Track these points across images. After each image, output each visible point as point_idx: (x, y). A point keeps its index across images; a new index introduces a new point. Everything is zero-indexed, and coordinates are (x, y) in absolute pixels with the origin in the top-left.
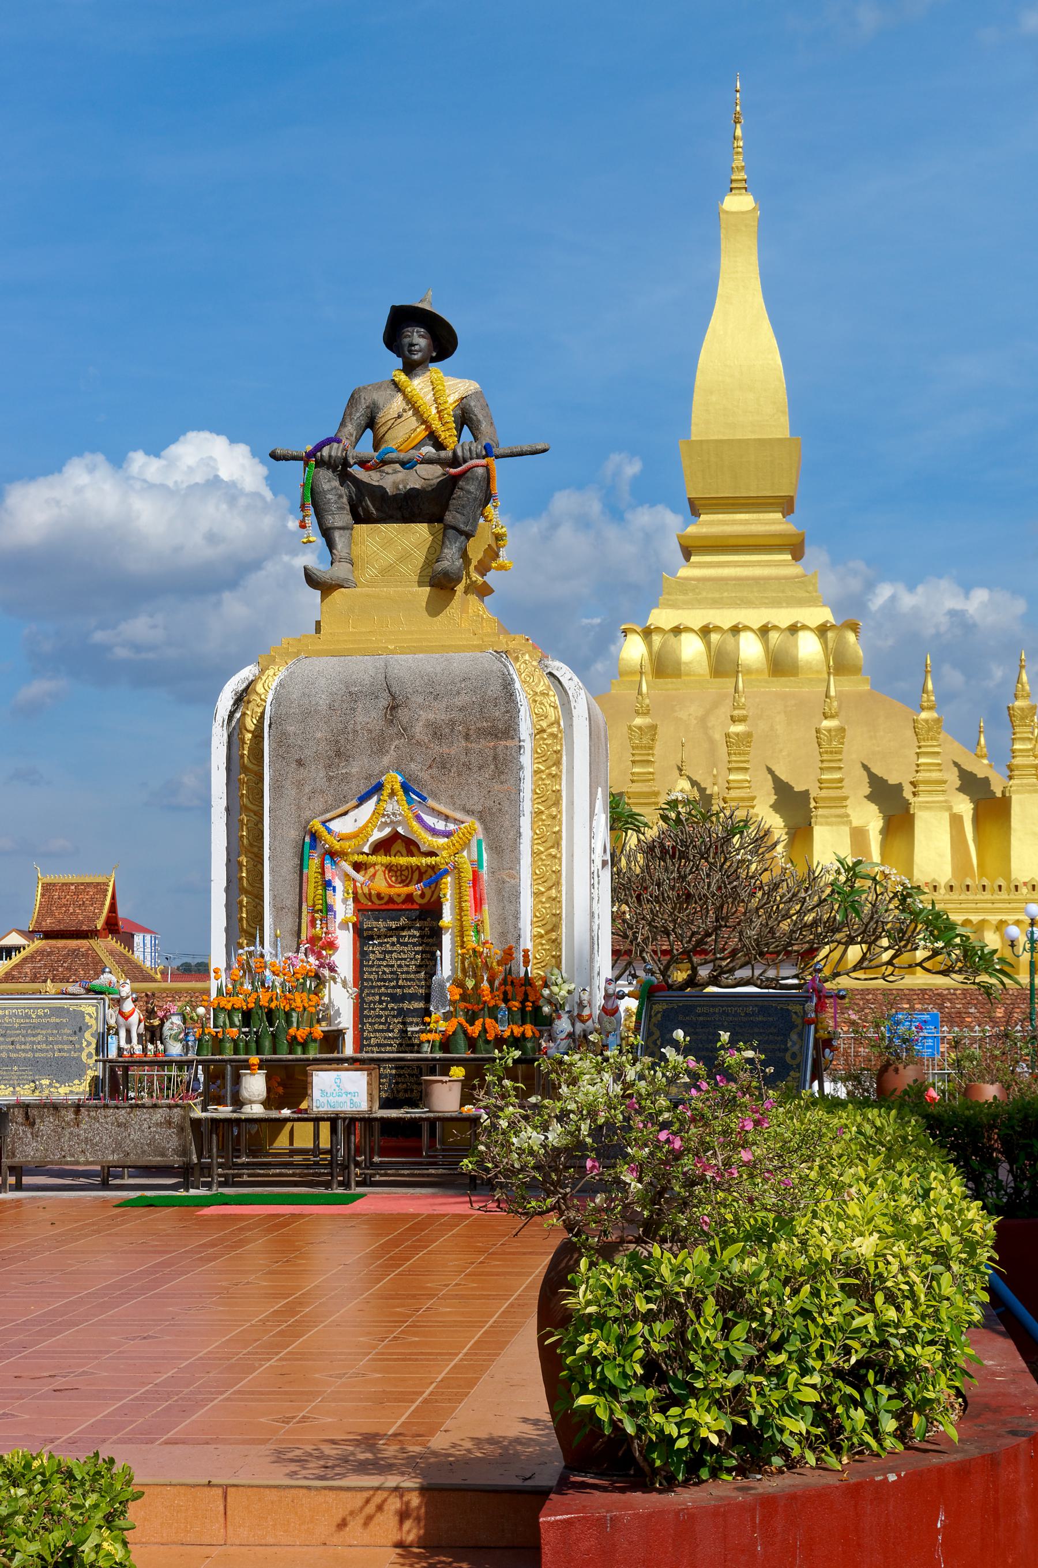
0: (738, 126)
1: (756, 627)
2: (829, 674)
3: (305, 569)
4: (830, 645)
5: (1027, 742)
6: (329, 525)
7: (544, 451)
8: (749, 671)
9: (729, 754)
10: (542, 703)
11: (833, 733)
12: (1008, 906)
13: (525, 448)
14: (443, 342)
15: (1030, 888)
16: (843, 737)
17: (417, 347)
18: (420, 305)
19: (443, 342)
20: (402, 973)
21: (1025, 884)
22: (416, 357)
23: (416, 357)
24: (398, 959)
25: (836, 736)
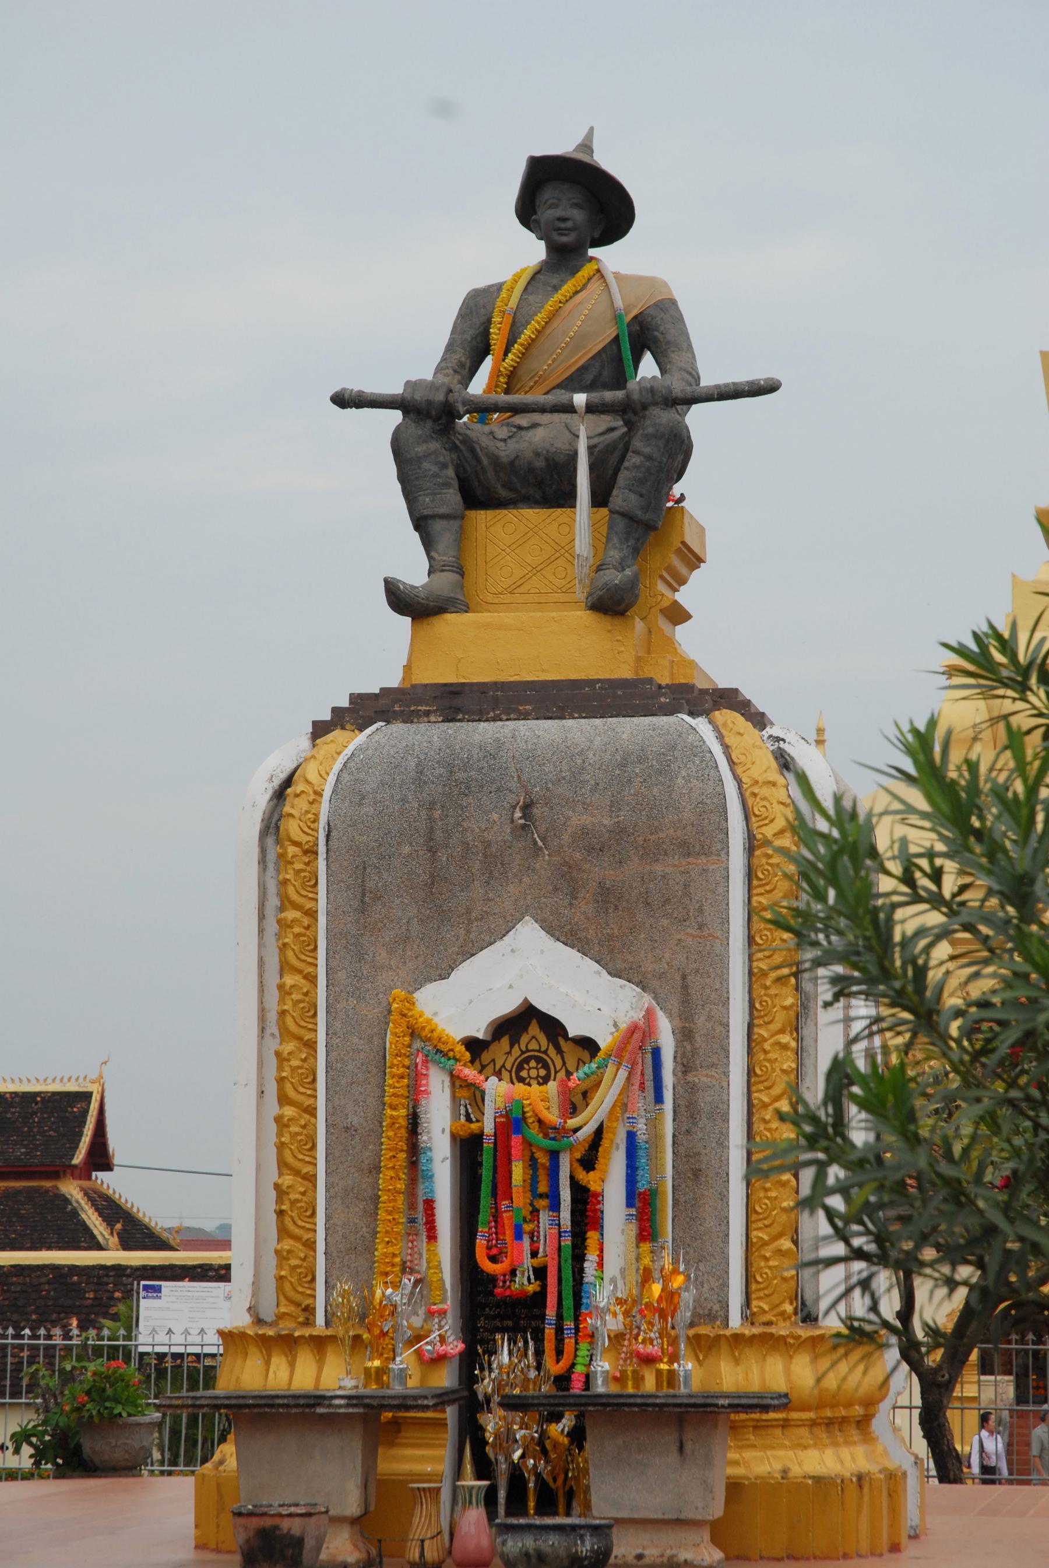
7: (770, 388)
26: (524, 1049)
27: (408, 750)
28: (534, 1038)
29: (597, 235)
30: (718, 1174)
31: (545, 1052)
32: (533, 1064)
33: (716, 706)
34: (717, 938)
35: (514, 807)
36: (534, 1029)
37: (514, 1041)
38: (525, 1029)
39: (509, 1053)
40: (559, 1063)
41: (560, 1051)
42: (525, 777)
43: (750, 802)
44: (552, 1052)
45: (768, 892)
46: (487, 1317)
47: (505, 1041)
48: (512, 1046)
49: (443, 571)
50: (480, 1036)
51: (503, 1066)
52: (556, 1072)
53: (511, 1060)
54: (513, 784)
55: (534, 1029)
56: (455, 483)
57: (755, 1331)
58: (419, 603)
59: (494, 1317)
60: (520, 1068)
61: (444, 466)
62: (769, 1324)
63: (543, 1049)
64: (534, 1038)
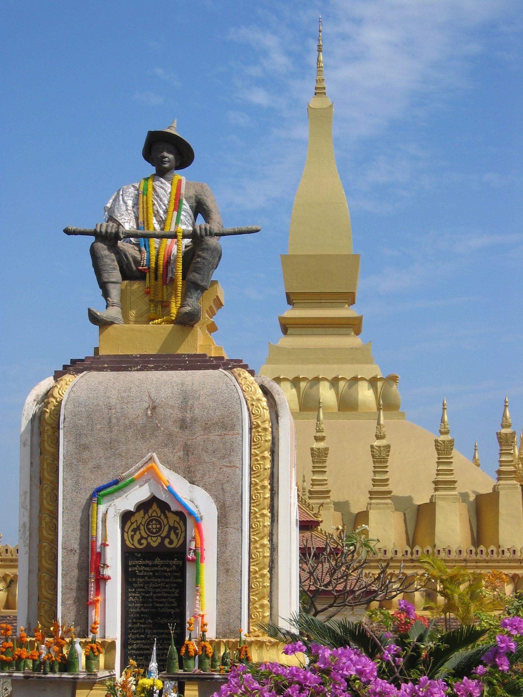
0: (321, 54)
1: (330, 379)
2: (379, 409)
3: (89, 310)
4: (379, 390)
5: (510, 456)
6: (106, 280)
7: (257, 231)
8: (325, 408)
9: (313, 462)
10: (257, 407)
11: (382, 449)
12: (497, 564)
13: (244, 228)
14: (184, 155)
15: (512, 552)
16: (389, 451)
17: (167, 159)
18: (168, 131)
19: (184, 155)
20: (156, 598)
21: (509, 549)
22: (166, 165)
23: (166, 165)
24: (153, 588)
25: (384, 450)
26: (150, 515)
27: (100, 383)
28: (155, 510)
29: (178, 165)
30: (237, 571)
31: (160, 517)
32: (154, 522)
33: (234, 367)
34: (238, 467)
35: (147, 409)
36: (155, 507)
37: (146, 512)
38: (151, 507)
39: (143, 517)
40: (166, 522)
41: (166, 517)
42: (152, 395)
43: (250, 408)
44: (163, 517)
45: (259, 448)
46: (133, 634)
47: (142, 512)
48: (145, 514)
49: (113, 306)
50: (132, 510)
51: (141, 523)
52: (164, 526)
53: (144, 520)
54: (147, 399)
55: (155, 507)
56: (118, 268)
57: (253, 639)
58: (103, 319)
59: (136, 634)
60: (148, 524)
61: (113, 261)
62: (258, 636)
63: (159, 515)
64: (155, 510)
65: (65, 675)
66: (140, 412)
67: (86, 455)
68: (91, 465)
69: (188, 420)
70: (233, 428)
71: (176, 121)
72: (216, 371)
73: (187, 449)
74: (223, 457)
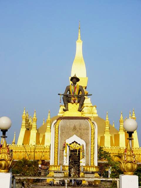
7: (91, 95)
36: (75, 143)
55: (75, 143)
65: (71, 179)
66: (73, 127)
67: (63, 134)
68: (64, 136)
69: (81, 128)
70: (88, 130)
71: (79, 45)
72: (90, 101)
73: (81, 133)
74: (87, 135)
